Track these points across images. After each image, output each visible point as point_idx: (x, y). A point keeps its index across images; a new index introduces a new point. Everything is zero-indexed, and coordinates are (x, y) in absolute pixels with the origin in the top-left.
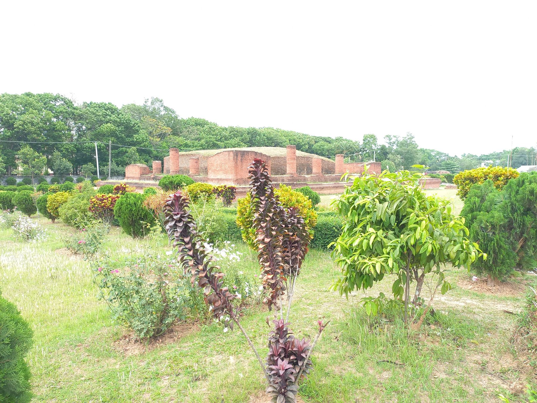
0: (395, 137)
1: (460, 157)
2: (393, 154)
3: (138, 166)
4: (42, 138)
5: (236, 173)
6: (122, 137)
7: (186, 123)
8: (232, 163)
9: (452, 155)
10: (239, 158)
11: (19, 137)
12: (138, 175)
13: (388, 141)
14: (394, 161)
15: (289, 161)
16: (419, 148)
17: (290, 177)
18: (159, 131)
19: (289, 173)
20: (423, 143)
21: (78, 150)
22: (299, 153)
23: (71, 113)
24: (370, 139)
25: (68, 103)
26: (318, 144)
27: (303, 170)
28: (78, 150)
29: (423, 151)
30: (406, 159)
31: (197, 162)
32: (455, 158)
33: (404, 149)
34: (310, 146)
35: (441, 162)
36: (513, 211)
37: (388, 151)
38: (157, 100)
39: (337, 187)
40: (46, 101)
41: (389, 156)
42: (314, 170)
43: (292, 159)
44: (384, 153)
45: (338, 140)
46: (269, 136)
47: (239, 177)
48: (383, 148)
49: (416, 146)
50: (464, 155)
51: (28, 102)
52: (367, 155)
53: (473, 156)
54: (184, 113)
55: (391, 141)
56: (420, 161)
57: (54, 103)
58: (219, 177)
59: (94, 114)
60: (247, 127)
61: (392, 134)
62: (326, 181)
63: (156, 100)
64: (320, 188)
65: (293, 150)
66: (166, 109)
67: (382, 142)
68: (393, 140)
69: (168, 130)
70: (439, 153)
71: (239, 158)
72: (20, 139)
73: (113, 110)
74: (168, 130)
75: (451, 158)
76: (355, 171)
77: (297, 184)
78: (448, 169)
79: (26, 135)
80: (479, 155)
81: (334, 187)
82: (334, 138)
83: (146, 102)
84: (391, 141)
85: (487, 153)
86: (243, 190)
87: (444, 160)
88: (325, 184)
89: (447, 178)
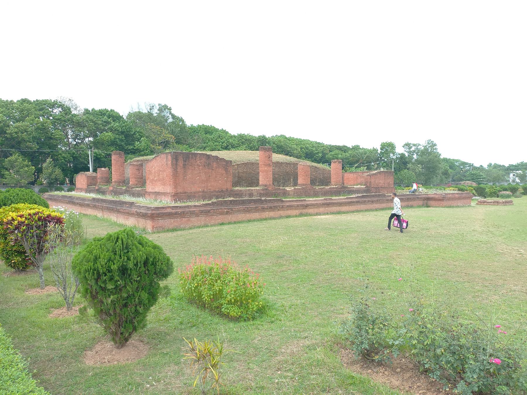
0: (414, 145)
1: (485, 166)
2: (413, 164)
3: (86, 175)
4: (35, 146)
5: (176, 185)
6: (121, 145)
7: (195, 130)
8: (169, 171)
9: (477, 165)
10: (181, 163)
11: (15, 143)
12: (85, 187)
13: (408, 150)
14: (414, 170)
15: (262, 168)
16: (442, 157)
17: (263, 190)
18: (161, 139)
19: (262, 185)
20: (446, 152)
21: (75, 158)
22: (277, 157)
23: (67, 117)
24: (388, 147)
25: (66, 110)
26: (333, 153)
27: (289, 180)
28: (75, 158)
29: (446, 160)
30: (428, 168)
31: (138, 170)
32: (481, 168)
33: (425, 158)
34: (324, 154)
35: (465, 173)
36: (433, 163)
37: (407, 160)
38: (166, 107)
39: (328, 205)
40: (43, 107)
41: (409, 166)
42: (300, 181)
43: (266, 165)
44: (403, 162)
45: (356, 148)
46: (279, 144)
47: (180, 190)
48: (402, 155)
49: (438, 155)
50: (490, 165)
51: (26, 108)
52: (385, 164)
53: (500, 166)
54: (192, 119)
55: (411, 150)
56: (443, 170)
57: (51, 110)
58: (157, 190)
59: (93, 122)
60: (257, 135)
61: (412, 142)
62: (316, 195)
63: (164, 108)
64: (302, 206)
65: (267, 153)
66: (174, 116)
67: (400, 150)
68: (413, 149)
69: (171, 138)
70: (464, 164)
71: (181, 163)
72: (13, 147)
73: (114, 116)
74: (171, 138)
75: (475, 168)
76: (359, 182)
77: (265, 200)
78: (473, 180)
79: (19, 143)
80: (507, 165)
81: (324, 205)
82: (351, 147)
83: (150, 109)
84: (411, 150)
85: (514, 163)
86: (173, 211)
87: (469, 170)
88: (311, 200)
89: (476, 191)
